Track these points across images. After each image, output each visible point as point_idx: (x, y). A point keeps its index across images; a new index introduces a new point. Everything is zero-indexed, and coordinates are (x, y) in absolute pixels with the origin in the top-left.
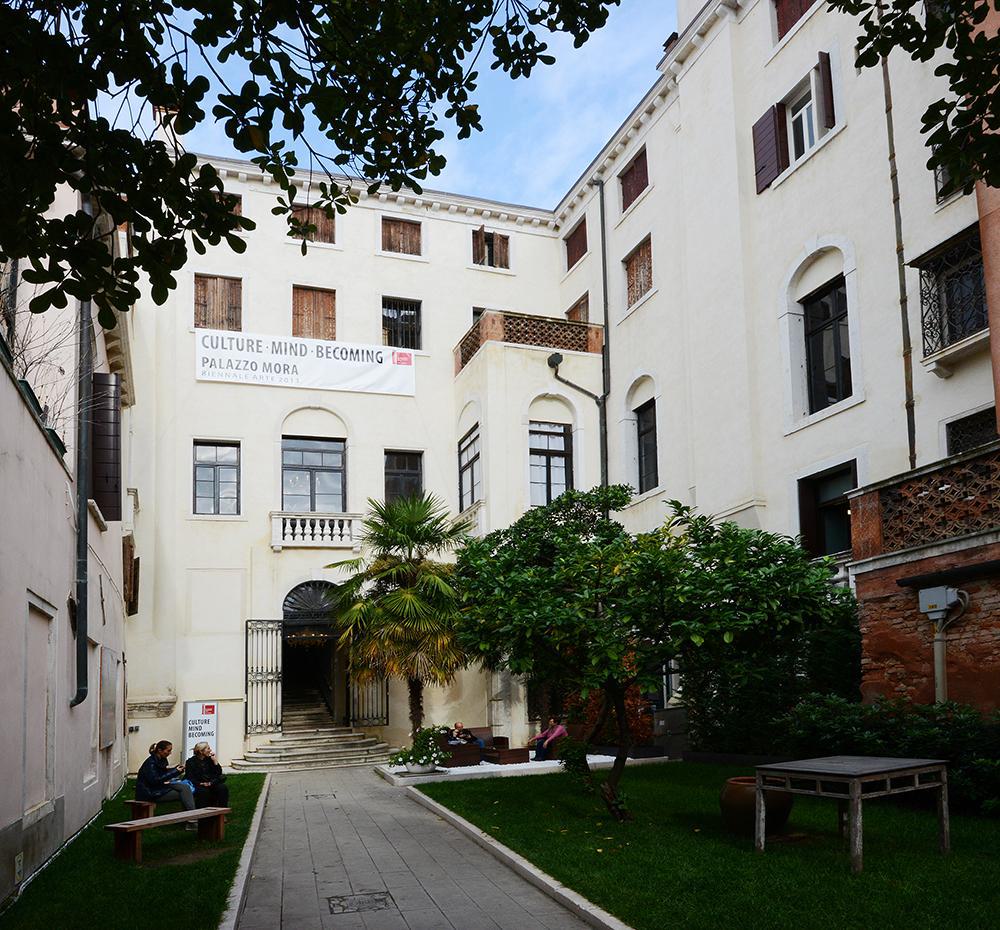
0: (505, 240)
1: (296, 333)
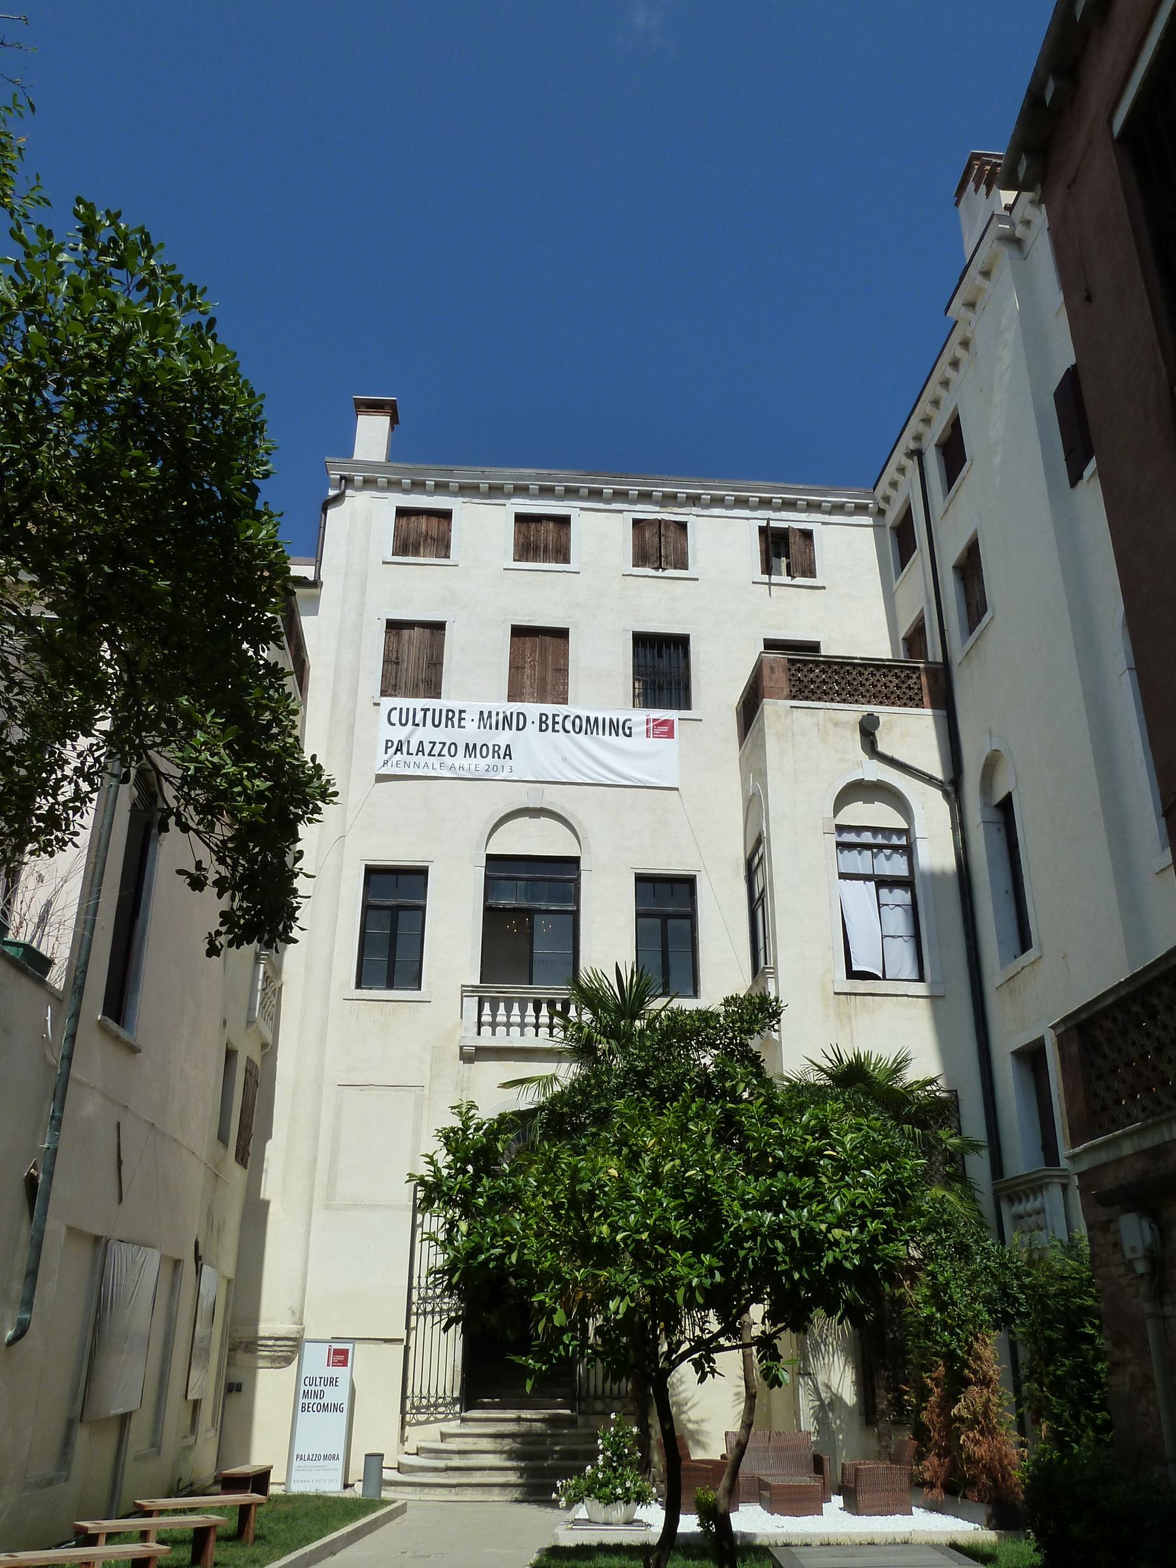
0: (807, 535)
1: (513, 696)
